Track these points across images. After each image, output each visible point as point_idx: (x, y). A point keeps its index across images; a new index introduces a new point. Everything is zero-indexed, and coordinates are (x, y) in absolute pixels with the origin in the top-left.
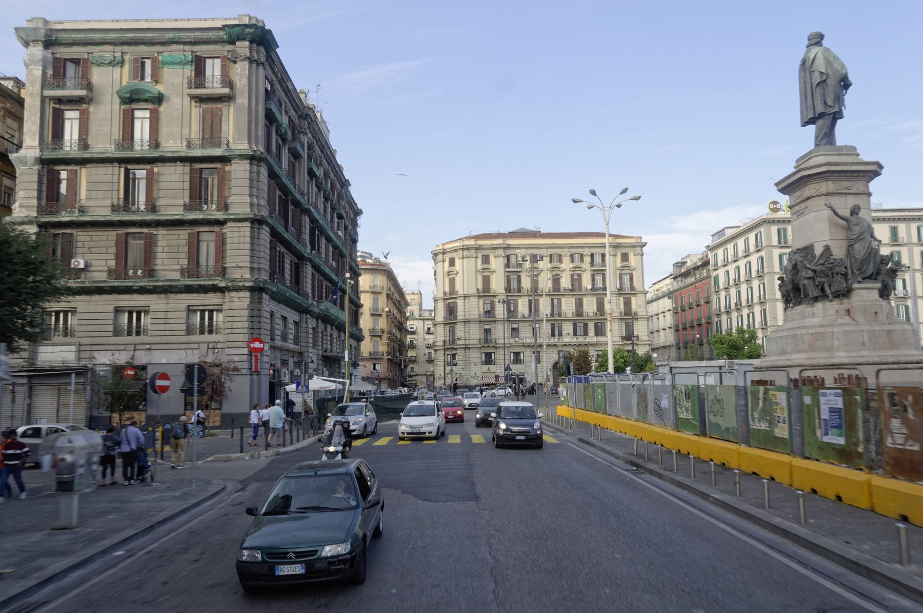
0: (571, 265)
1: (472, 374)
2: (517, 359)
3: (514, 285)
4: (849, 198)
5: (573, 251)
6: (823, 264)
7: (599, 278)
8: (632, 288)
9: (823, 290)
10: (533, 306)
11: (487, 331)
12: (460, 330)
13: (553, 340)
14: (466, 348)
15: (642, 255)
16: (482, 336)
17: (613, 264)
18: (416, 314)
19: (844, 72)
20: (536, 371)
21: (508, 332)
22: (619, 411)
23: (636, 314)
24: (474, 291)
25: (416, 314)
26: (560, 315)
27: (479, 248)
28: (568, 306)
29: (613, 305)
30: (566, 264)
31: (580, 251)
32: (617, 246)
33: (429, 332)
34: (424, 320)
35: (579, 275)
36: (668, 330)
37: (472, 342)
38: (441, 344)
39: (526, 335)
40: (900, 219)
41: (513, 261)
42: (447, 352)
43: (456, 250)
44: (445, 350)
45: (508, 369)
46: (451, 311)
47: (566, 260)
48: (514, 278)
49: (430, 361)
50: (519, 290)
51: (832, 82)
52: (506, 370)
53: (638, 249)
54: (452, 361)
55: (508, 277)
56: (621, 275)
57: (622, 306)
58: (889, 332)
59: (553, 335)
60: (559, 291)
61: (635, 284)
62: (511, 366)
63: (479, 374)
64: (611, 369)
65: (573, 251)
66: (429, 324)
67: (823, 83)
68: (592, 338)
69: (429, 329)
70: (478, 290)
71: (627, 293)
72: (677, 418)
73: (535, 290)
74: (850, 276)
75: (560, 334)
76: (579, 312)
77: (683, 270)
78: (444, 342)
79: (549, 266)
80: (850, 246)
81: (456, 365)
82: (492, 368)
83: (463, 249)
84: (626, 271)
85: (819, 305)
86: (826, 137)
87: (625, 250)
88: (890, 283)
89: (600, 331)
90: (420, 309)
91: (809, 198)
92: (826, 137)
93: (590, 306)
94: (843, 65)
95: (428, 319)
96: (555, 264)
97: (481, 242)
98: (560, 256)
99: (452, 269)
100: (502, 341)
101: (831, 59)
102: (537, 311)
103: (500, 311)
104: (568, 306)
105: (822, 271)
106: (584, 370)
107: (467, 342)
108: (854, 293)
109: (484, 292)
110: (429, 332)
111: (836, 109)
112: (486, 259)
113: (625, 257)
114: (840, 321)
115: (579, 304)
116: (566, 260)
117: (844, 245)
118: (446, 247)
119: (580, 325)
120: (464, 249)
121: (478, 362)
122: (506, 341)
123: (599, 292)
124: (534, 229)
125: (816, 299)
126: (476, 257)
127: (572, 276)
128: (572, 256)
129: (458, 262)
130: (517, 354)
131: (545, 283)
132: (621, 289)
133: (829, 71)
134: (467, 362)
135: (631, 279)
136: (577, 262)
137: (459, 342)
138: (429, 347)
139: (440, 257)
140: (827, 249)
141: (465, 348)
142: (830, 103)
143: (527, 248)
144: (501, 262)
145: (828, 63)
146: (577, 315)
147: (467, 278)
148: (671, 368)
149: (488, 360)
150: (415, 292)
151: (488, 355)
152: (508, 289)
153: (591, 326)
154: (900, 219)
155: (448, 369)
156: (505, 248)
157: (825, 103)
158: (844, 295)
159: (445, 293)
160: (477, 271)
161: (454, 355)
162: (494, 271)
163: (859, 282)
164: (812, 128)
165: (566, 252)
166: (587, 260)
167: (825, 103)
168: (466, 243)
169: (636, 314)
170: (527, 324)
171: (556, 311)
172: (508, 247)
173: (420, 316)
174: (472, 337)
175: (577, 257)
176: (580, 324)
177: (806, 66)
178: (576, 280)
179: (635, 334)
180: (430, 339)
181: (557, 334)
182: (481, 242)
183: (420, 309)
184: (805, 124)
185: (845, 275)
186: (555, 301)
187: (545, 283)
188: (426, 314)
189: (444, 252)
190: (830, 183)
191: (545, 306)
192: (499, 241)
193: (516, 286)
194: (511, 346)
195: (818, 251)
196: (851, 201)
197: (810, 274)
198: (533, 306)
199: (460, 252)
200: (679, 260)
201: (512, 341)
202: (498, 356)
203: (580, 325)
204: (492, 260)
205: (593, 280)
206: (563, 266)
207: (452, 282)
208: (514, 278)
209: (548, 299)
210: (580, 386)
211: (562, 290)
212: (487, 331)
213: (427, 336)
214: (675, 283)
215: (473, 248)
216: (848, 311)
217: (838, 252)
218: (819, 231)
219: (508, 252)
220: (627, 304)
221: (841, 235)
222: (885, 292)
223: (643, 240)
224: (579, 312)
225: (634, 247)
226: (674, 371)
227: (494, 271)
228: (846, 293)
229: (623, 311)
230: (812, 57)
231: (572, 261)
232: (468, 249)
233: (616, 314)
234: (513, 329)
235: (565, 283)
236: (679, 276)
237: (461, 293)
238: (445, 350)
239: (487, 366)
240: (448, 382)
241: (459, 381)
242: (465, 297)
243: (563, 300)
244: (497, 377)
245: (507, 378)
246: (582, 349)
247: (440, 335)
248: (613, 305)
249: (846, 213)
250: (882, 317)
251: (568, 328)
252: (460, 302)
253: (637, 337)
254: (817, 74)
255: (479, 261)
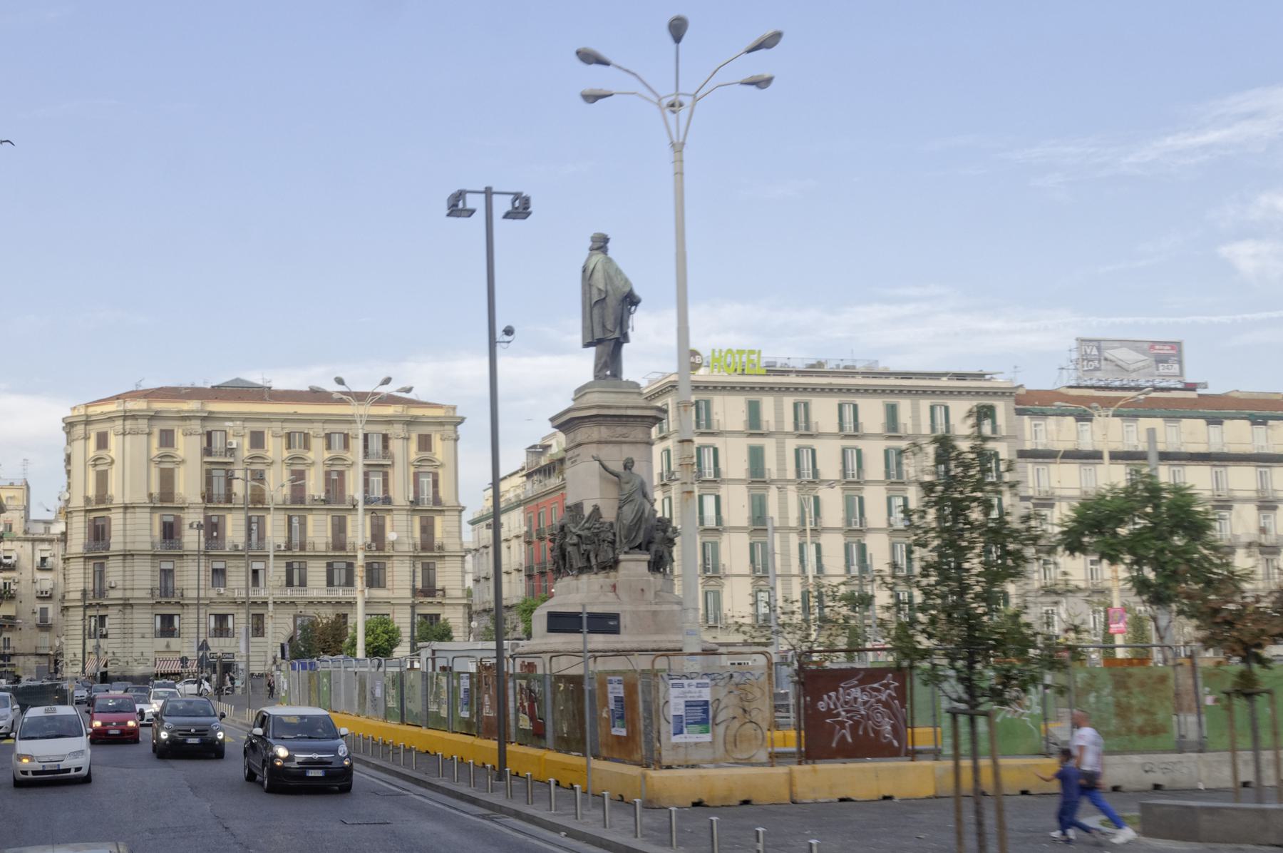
0: (327, 455)
1: (136, 655)
2: (221, 629)
3: (219, 488)
4: (625, 447)
5: (330, 428)
6: (589, 529)
7: (376, 480)
8: (436, 500)
9: (588, 559)
10: (254, 528)
11: (167, 574)
12: (114, 572)
13: (290, 593)
14: (126, 605)
15: (456, 440)
16: (157, 584)
17: (404, 451)
18: (18, 529)
19: (627, 289)
20: (256, 653)
21: (206, 577)
22: (343, 707)
23: (441, 548)
24: (142, 498)
25: (18, 529)
26: (303, 548)
27: (154, 417)
28: (318, 530)
29: (402, 531)
30: (318, 452)
31: (344, 428)
32: (411, 422)
33: (43, 565)
34: (34, 541)
35: (341, 474)
36: (514, 573)
37: (137, 594)
38: (78, 595)
39: (237, 580)
40: (901, 392)
41: (218, 442)
42: (89, 613)
43: (111, 419)
44: (86, 607)
45: (203, 647)
46: (99, 533)
47: (318, 444)
48: (219, 474)
49: (44, 626)
50: (229, 499)
51: (612, 302)
52: (200, 648)
53: (449, 428)
54: (98, 630)
55: (208, 472)
56: (416, 476)
57: (417, 534)
58: (655, 613)
59: (289, 583)
60: (303, 502)
61: (442, 494)
62: (211, 642)
63: (149, 654)
64: (360, 653)
65: (330, 428)
66: (43, 550)
67: (602, 301)
68: (360, 592)
69: (43, 559)
70: (150, 495)
71: (427, 509)
72: (387, 708)
73: (257, 500)
74: (617, 545)
75: (303, 583)
76: (339, 542)
77: (544, 461)
78: (84, 592)
79: (286, 454)
80: (620, 508)
81: (105, 636)
82: (174, 643)
83: (125, 418)
84: (426, 468)
85: (584, 578)
86: (610, 362)
87: (425, 430)
88: (666, 554)
89: (375, 578)
90: (27, 520)
91: (580, 445)
92: (610, 362)
93: (358, 530)
94: (626, 281)
95: (43, 540)
96: (297, 451)
97: (158, 406)
98: (306, 436)
99: (102, 453)
100: (194, 594)
101: (612, 273)
102: (261, 538)
103: (192, 539)
104: (318, 530)
105: (587, 537)
106: (334, 650)
107: (128, 594)
108: (622, 565)
109: (162, 500)
110: (43, 565)
111: (617, 335)
112: (167, 438)
113: (425, 443)
114: (602, 599)
115: (339, 528)
116: (318, 444)
117: (616, 504)
118: (92, 410)
119: (340, 566)
120: (126, 417)
121: (149, 631)
122: (202, 594)
123: (379, 508)
124: (260, 382)
125: (581, 571)
126: (149, 434)
127: (328, 474)
128: (328, 437)
129: (114, 441)
130: (222, 618)
131: (277, 485)
132: (416, 502)
133: (609, 288)
134: (127, 633)
135: (435, 484)
136: (337, 451)
137: (112, 594)
138: (45, 597)
139: (79, 430)
140: (596, 509)
141: (124, 605)
142: (609, 327)
143: (245, 420)
144: (197, 443)
145: (608, 278)
146: (335, 548)
147: (130, 478)
148: (434, 651)
149: (167, 628)
150: (17, 483)
151: (167, 620)
152: (208, 497)
153: (360, 573)
154: (901, 392)
155: (91, 643)
156: (204, 419)
157: (604, 326)
158: (611, 567)
159: (87, 500)
160: (150, 460)
161: (102, 618)
162: (183, 462)
163: (626, 553)
164: (592, 350)
165: (317, 429)
166: (357, 445)
167: (604, 326)
168: (132, 405)
169: (441, 548)
170: (242, 563)
171: (296, 539)
172: (209, 417)
173: (26, 532)
174: (137, 584)
175: (337, 440)
176: (340, 569)
177: (587, 275)
178: (335, 484)
179: (439, 585)
180: (46, 581)
181: (296, 582)
182: (158, 406)
183: (27, 520)
184: (587, 345)
185: (613, 543)
186: (295, 521)
187: (277, 485)
188: (39, 530)
189: (88, 422)
190: (603, 429)
191: (275, 530)
192: (192, 406)
193: (222, 491)
194: (212, 603)
195: (587, 511)
196: (628, 452)
197: (575, 540)
198: (254, 528)
199: (119, 423)
200: (538, 442)
201: (212, 593)
202: (187, 621)
203: (340, 566)
204: (180, 439)
205: (366, 482)
206: (311, 455)
207: (102, 479)
208: (219, 474)
209: (281, 518)
210: (305, 674)
211: (308, 500)
212: (167, 574)
213: (39, 575)
214: (529, 486)
215: (143, 417)
216: (614, 587)
217: (609, 515)
218: (587, 488)
219: (210, 426)
220: (427, 529)
221: (613, 492)
222: (659, 564)
223: (459, 413)
224: (339, 542)
225: (441, 424)
226: (437, 654)
227: (183, 462)
228: (613, 565)
229: (418, 541)
230: (591, 267)
231: (329, 447)
232: (134, 417)
233: (406, 548)
234: (215, 571)
235: (315, 486)
236: (538, 471)
237: (118, 500)
238: (86, 607)
239: (164, 641)
240: (91, 668)
241: (110, 667)
242: (126, 508)
243: (311, 519)
244: (184, 661)
245: (202, 662)
246: (342, 611)
247: (78, 579)
248: (402, 531)
249: (617, 466)
250: (650, 595)
251: (316, 573)
252: (116, 518)
253: (443, 590)
254: (595, 291)
255: (155, 441)
